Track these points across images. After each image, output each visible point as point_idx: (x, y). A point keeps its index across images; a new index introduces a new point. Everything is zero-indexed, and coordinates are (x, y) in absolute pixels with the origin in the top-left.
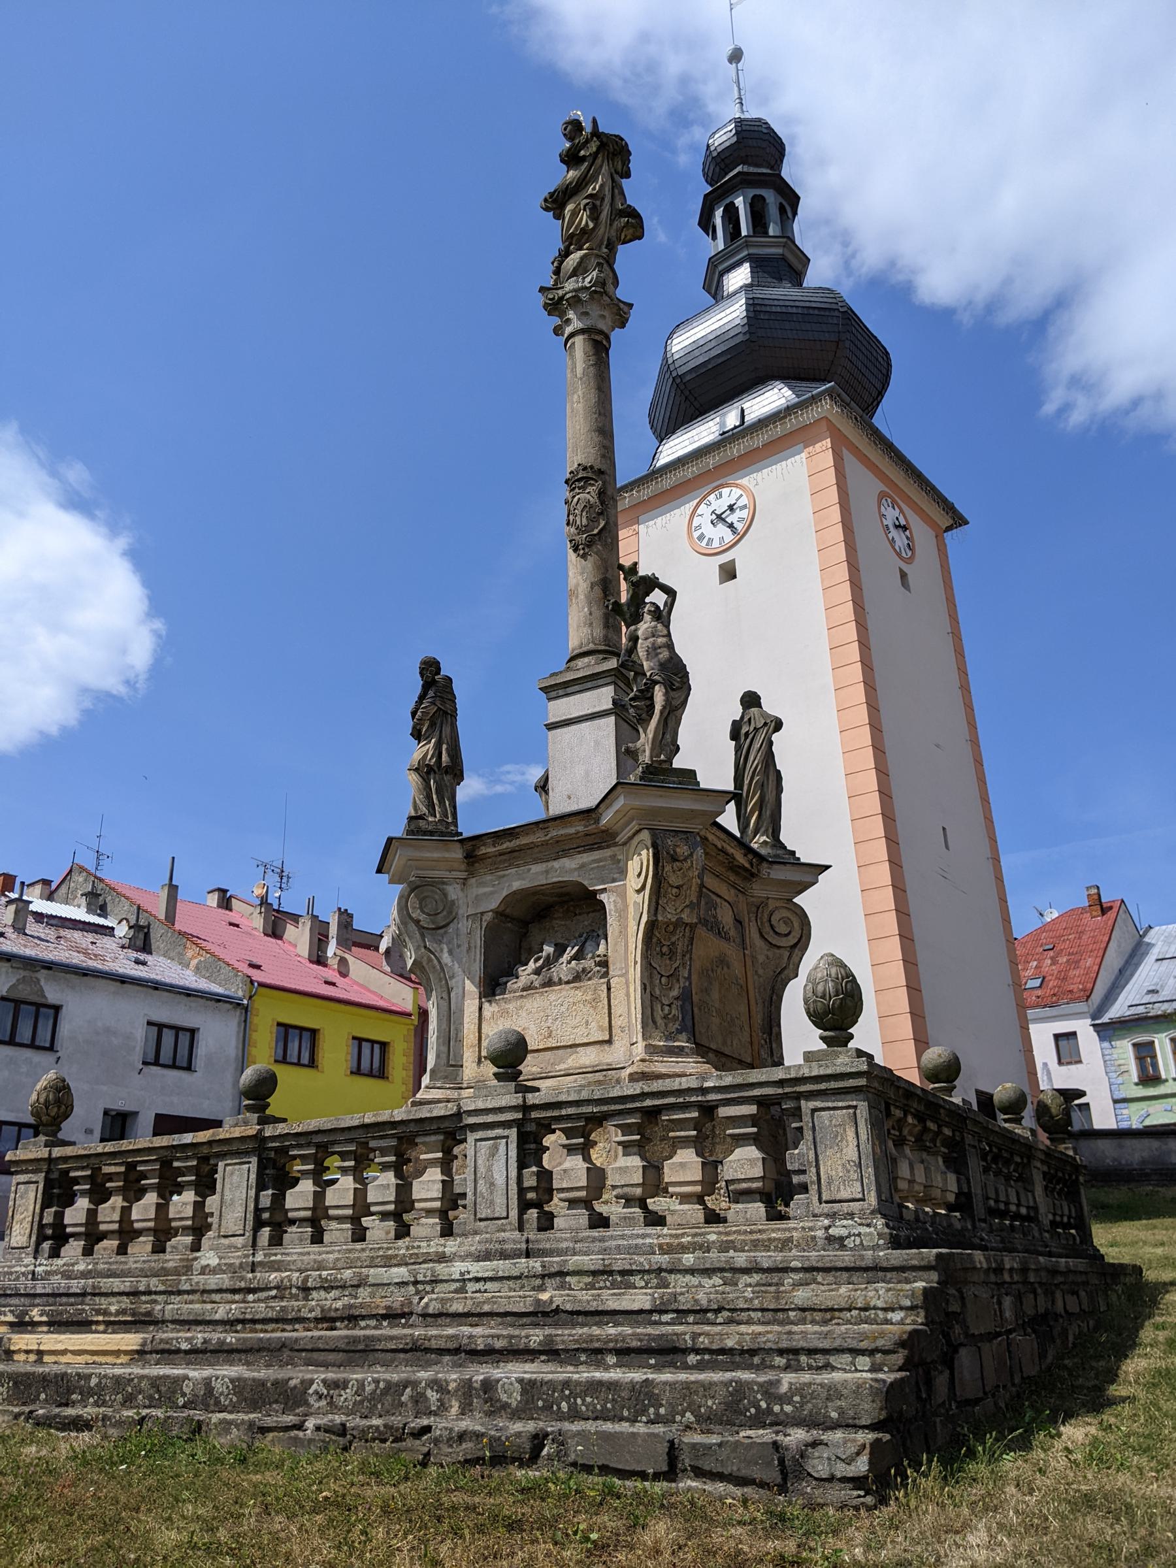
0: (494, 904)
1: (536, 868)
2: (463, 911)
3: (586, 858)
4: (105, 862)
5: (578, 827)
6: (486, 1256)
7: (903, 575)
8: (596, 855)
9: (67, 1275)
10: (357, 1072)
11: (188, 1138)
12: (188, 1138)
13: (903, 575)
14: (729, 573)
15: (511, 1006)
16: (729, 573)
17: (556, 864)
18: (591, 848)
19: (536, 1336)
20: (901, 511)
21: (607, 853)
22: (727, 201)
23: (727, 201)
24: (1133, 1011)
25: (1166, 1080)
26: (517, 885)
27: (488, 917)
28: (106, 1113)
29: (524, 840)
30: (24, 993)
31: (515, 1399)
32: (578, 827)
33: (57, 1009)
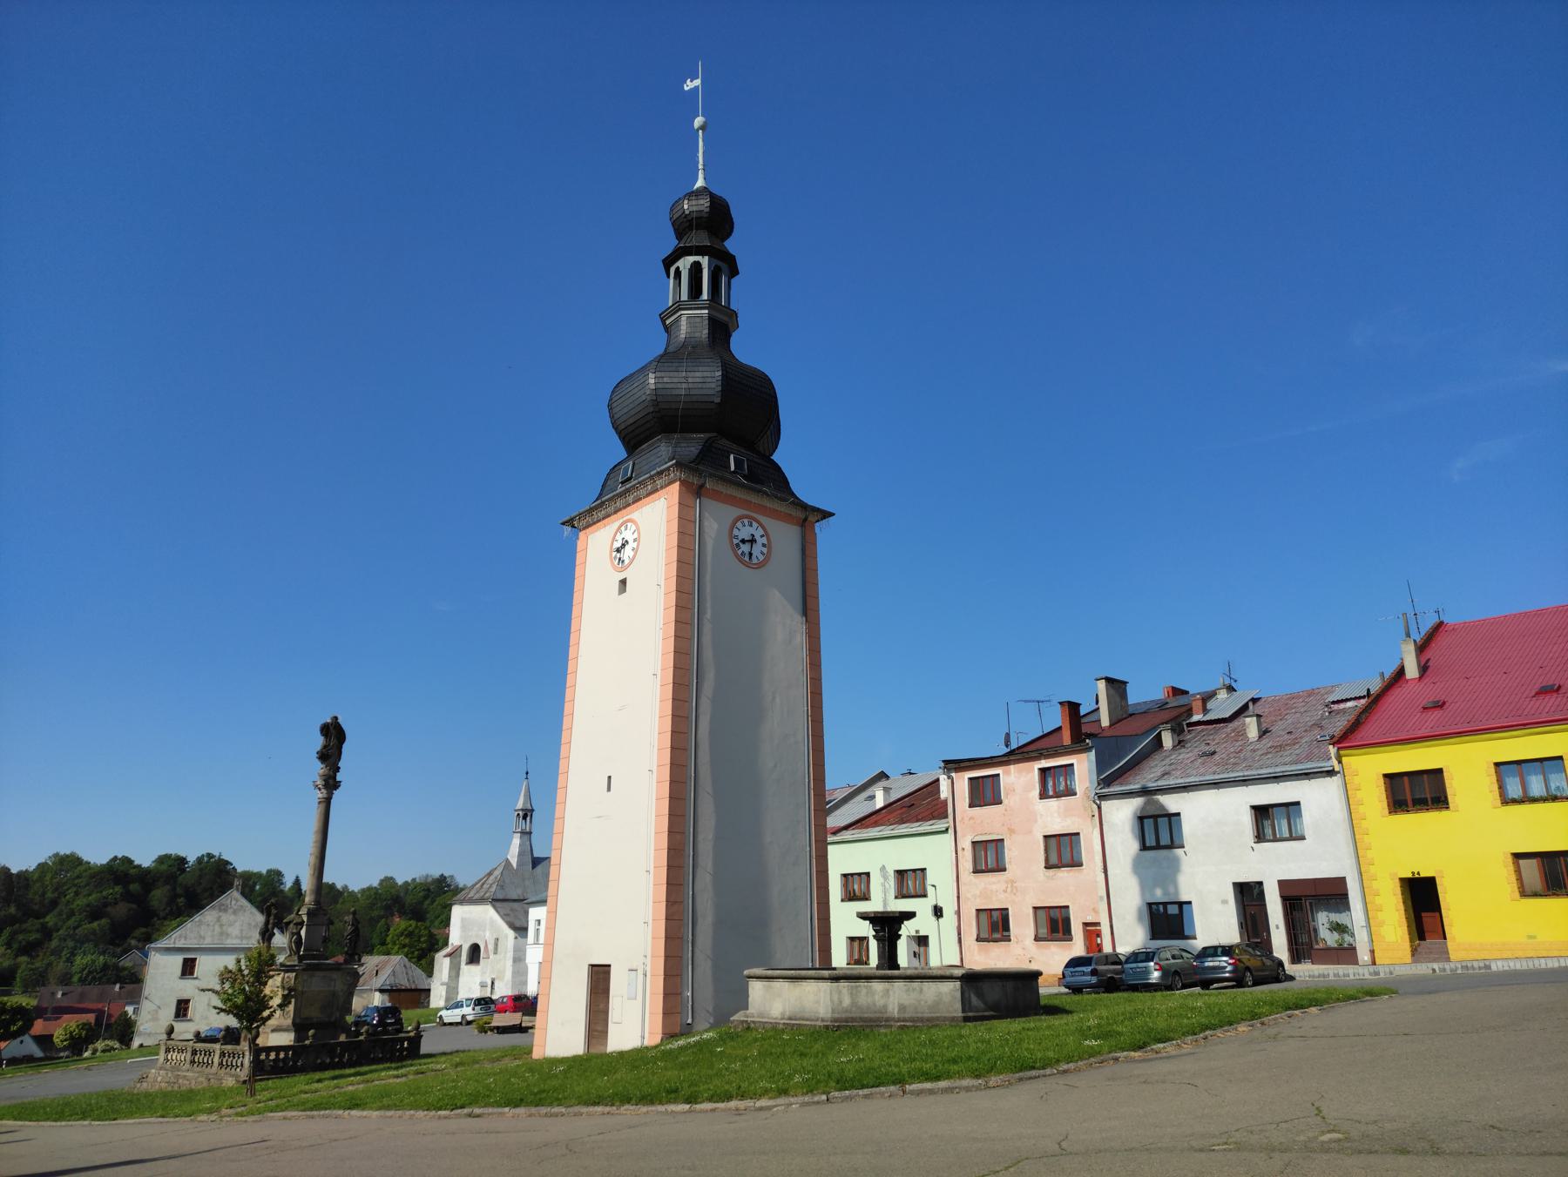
28: (1235, 884)
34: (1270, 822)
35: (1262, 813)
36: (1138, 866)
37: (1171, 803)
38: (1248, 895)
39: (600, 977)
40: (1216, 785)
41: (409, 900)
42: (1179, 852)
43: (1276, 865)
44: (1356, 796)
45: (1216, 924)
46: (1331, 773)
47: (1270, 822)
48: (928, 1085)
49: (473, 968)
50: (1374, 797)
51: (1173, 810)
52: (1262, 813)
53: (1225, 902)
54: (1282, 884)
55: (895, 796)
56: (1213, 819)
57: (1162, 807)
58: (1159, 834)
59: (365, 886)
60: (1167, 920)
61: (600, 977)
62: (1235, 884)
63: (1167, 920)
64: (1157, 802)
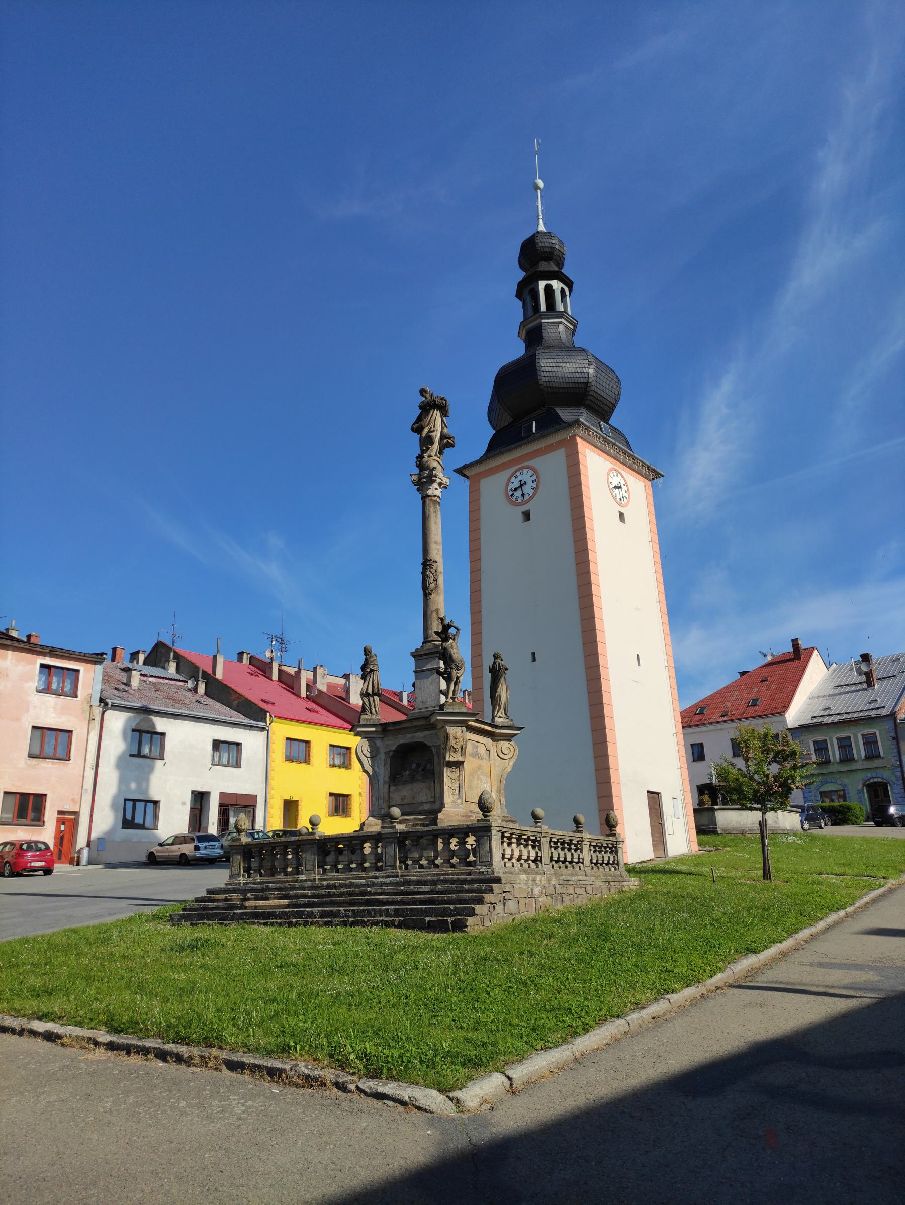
0: (393, 748)
1: (409, 736)
2: (382, 750)
3: (426, 733)
4: (177, 640)
5: (422, 723)
6: (388, 877)
7: (622, 515)
8: (430, 732)
9: (254, 883)
10: (333, 765)
11: (293, 839)
12: (293, 839)
13: (622, 515)
14: (527, 516)
15: (400, 787)
16: (527, 516)
17: (416, 735)
18: (428, 730)
19: (399, 898)
20: (623, 476)
21: (434, 732)
22: (531, 286)
23: (531, 286)
24: (815, 721)
25: (857, 761)
26: (402, 742)
27: (391, 753)
28: (193, 792)
29: (404, 726)
30: (144, 727)
31: (392, 913)
32: (422, 723)
33: (163, 734)
34: (226, 752)
35: (217, 745)
36: (121, 764)
37: (161, 724)
38: (200, 799)
39: (654, 798)
40: (197, 719)
41: (507, 419)
42: (159, 763)
43: (222, 782)
44: (272, 746)
45: (173, 822)
46: (263, 729)
47: (226, 752)
48: (789, 943)
49: (35, 679)
50: (279, 749)
51: (159, 729)
52: (217, 745)
53: (183, 804)
54: (223, 795)
55: (147, 653)
56: (187, 741)
57: (153, 725)
58: (145, 743)
59: (565, 263)
60: (136, 812)
61: (654, 798)
62: (193, 792)
63: (136, 812)
64: (151, 721)
